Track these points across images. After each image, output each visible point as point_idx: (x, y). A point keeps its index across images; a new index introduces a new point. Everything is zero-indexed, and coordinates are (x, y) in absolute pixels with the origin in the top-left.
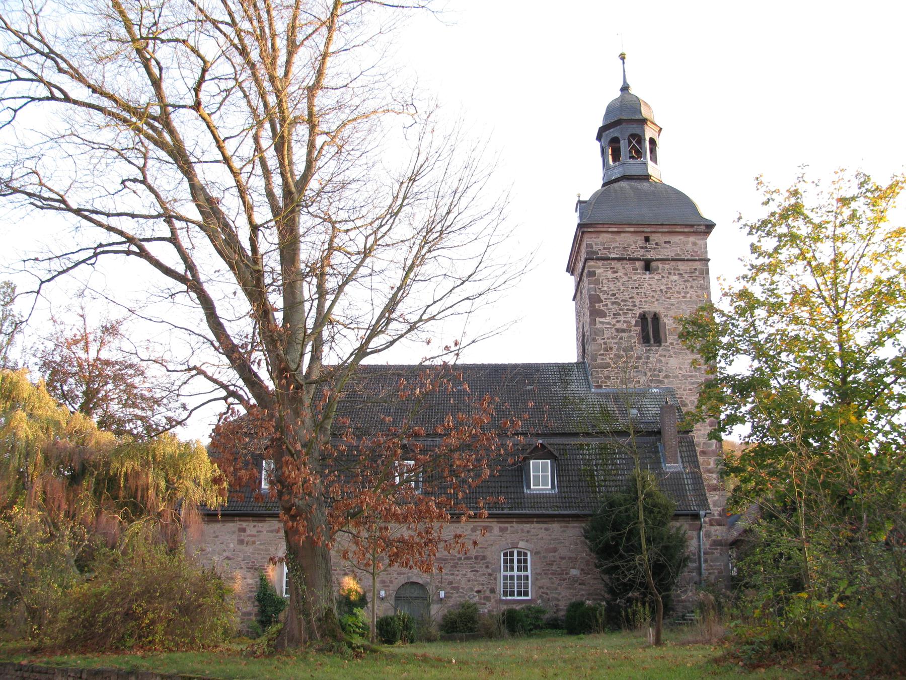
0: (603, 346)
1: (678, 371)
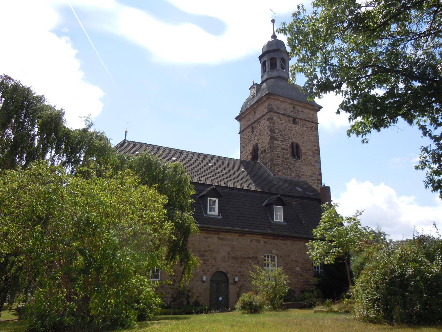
0: (277, 155)
1: (307, 173)
